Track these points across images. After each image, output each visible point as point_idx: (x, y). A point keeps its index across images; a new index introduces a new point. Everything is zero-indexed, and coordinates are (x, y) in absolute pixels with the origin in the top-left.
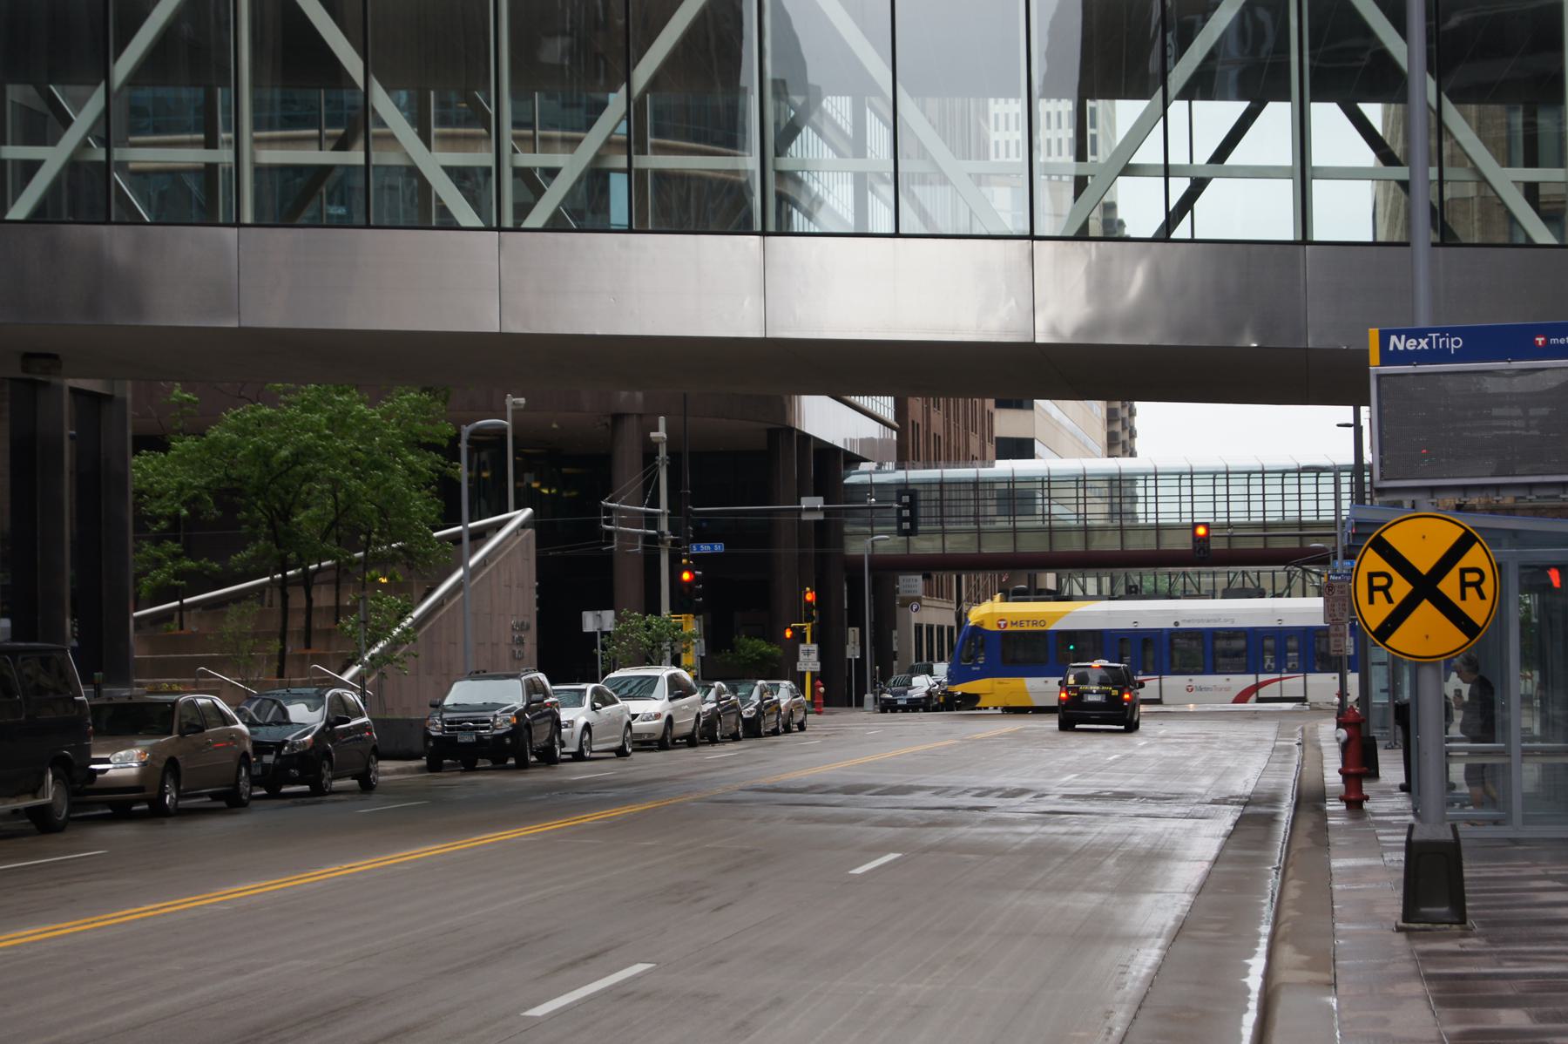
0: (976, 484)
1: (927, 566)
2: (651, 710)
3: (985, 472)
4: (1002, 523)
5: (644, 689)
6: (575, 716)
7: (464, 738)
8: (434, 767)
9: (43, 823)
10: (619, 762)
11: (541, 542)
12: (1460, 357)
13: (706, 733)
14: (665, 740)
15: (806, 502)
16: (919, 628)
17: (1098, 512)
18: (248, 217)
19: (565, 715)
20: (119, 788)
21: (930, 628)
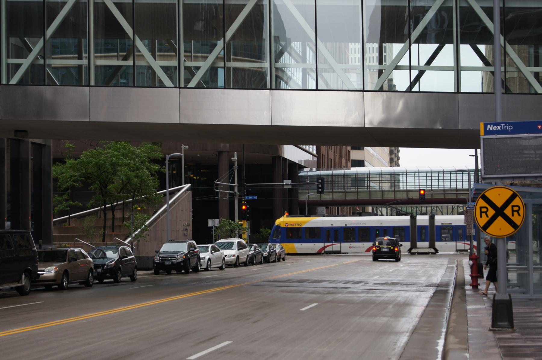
0: (344, 176)
2: (231, 253)
3: (347, 172)
4: (353, 189)
5: (229, 246)
6: (205, 256)
8: (156, 273)
9: (21, 292)
10: (220, 272)
11: (194, 195)
12: (512, 132)
14: (236, 264)
15: (285, 182)
17: (386, 186)
18: (93, 83)
19: (202, 255)
20: (47, 280)
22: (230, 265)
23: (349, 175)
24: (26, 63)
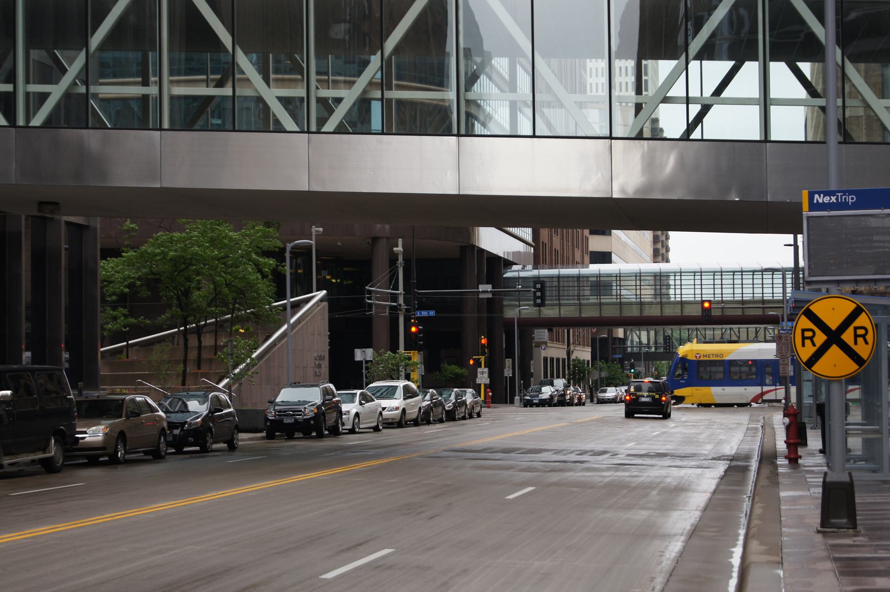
0: (579, 277)
1: (550, 324)
2: (393, 405)
3: (584, 271)
4: (593, 300)
5: (389, 393)
7: (287, 420)
8: (270, 436)
11: (331, 310)
12: (854, 206)
13: (425, 418)
14: (401, 422)
15: (482, 287)
16: (545, 359)
17: (647, 294)
18: (166, 125)
19: (345, 407)
21: (552, 359)
22: (390, 424)
23: (587, 277)
24: (56, 91)
